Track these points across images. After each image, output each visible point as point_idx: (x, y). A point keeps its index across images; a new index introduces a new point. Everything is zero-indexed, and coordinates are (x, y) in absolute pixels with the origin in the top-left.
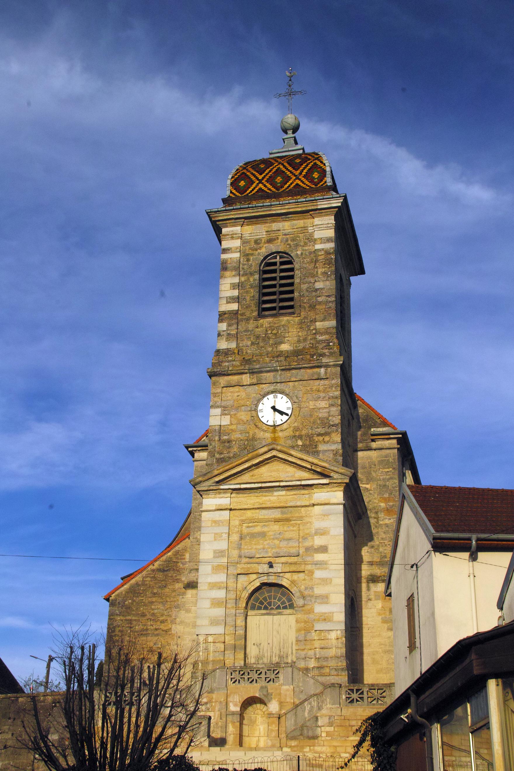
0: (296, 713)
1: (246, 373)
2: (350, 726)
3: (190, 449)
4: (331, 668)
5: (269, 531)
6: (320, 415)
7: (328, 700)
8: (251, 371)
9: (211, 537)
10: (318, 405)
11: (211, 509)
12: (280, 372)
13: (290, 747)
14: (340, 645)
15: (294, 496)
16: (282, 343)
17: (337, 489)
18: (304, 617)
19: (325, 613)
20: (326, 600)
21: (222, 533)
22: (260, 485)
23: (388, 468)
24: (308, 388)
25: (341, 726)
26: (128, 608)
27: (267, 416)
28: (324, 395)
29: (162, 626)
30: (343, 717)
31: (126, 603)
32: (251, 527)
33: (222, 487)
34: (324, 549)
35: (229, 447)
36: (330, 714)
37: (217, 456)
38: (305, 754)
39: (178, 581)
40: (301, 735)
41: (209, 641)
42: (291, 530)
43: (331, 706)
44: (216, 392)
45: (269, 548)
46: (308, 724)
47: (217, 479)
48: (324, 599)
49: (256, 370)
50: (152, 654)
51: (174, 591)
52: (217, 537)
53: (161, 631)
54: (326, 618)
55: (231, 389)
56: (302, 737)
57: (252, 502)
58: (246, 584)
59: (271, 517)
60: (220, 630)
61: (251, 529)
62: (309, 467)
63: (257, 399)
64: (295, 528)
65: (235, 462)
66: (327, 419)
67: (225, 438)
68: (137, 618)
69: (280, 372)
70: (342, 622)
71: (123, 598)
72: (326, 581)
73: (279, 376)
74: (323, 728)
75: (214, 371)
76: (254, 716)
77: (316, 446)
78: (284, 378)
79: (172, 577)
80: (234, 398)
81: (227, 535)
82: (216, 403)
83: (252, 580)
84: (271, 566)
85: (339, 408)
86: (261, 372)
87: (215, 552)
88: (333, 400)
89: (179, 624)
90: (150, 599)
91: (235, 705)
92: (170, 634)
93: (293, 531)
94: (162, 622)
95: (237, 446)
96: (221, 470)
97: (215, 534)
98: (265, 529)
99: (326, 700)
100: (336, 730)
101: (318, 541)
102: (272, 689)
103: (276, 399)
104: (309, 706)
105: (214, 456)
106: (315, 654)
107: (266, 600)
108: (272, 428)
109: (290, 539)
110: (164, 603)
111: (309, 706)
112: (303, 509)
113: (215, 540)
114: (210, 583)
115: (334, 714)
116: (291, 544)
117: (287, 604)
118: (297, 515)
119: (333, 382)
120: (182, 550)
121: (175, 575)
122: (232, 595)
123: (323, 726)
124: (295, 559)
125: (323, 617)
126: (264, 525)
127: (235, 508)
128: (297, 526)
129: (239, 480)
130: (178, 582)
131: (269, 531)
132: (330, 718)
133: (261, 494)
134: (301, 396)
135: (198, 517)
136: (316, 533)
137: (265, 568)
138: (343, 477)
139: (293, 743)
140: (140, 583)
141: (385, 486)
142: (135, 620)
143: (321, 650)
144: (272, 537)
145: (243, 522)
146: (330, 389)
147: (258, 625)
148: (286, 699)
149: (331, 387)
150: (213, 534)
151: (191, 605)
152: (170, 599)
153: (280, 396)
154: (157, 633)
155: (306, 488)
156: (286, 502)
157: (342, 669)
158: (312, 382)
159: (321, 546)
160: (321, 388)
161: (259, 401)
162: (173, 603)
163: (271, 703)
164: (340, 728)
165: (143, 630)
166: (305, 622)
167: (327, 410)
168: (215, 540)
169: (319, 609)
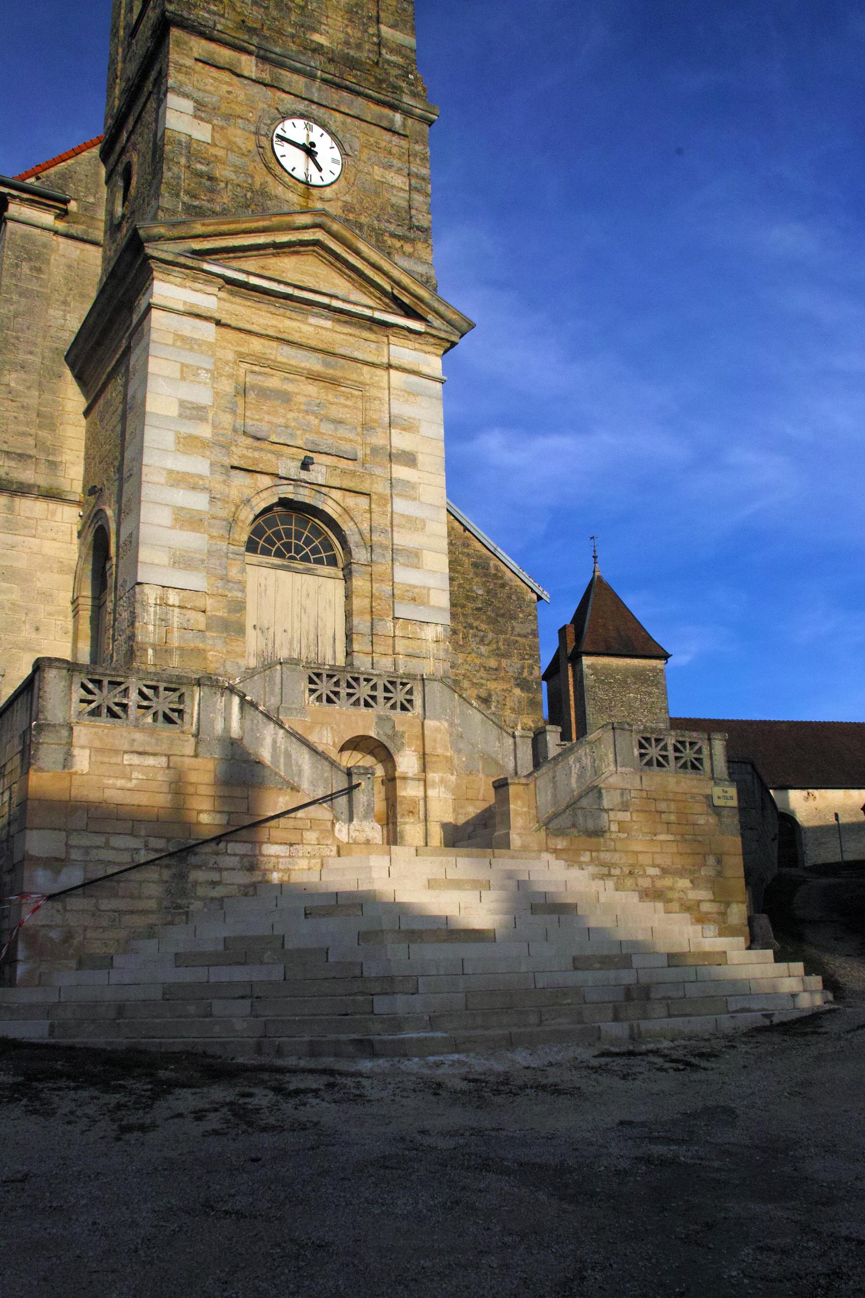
1: (250, 53)
2: (657, 812)
5: (299, 394)
6: (394, 200)
8: (262, 53)
9: (172, 370)
10: (389, 178)
11: (175, 307)
12: (318, 83)
14: (442, 654)
15: (348, 338)
16: (315, 30)
17: (431, 349)
19: (415, 587)
20: (416, 560)
22: (289, 290)
24: (372, 140)
28: (400, 165)
30: (644, 794)
32: (260, 373)
33: (206, 266)
40: (574, 826)
42: (340, 404)
44: (181, 61)
45: (298, 429)
47: (197, 245)
48: (413, 557)
49: (274, 56)
52: (187, 373)
54: (416, 598)
55: (214, 72)
56: (575, 832)
58: (248, 492)
59: (303, 365)
60: (196, 581)
61: (260, 377)
62: (388, 288)
65: (245, 222)
69: (318, 83)
73: (317, 91)
74: (611, 813)
75: (181, 16)
78: (326, 98)
84: (306, 465)
86: (282, 66)
87: (182, 404)
93: (346, 406)
96: (211, 229)
98: (290, 387)
99: (606, 755)
102: (403, 725)
105: (178, 195)
107: (280, 538)
108: (303, 186)
109: (341, 422)
112: (366, 369)
113: (183, 378)
114: (170, 472)
115: (629, 787)
116: (342, 432)
118: (354, 377)
123: (611, 810)
125: (410, 594)
126: (286, 379)
127: (229, 322)
129: (251, 264)
131: (297, 394)
132: (622, 795)
133: (282, 310)
135: (12, 341)
137: (290, 468)
138: (449, 329)
143: (408, 659)
144: (303, 407)
145: (242, 357)
148: (434, 748)
150: (179, 365)
155: (375, 328)
158: (377, 130)
159: (404, 451)
160: (395, 150)
163: (401, 753)
168: (183, 378)
169: (404, 576)
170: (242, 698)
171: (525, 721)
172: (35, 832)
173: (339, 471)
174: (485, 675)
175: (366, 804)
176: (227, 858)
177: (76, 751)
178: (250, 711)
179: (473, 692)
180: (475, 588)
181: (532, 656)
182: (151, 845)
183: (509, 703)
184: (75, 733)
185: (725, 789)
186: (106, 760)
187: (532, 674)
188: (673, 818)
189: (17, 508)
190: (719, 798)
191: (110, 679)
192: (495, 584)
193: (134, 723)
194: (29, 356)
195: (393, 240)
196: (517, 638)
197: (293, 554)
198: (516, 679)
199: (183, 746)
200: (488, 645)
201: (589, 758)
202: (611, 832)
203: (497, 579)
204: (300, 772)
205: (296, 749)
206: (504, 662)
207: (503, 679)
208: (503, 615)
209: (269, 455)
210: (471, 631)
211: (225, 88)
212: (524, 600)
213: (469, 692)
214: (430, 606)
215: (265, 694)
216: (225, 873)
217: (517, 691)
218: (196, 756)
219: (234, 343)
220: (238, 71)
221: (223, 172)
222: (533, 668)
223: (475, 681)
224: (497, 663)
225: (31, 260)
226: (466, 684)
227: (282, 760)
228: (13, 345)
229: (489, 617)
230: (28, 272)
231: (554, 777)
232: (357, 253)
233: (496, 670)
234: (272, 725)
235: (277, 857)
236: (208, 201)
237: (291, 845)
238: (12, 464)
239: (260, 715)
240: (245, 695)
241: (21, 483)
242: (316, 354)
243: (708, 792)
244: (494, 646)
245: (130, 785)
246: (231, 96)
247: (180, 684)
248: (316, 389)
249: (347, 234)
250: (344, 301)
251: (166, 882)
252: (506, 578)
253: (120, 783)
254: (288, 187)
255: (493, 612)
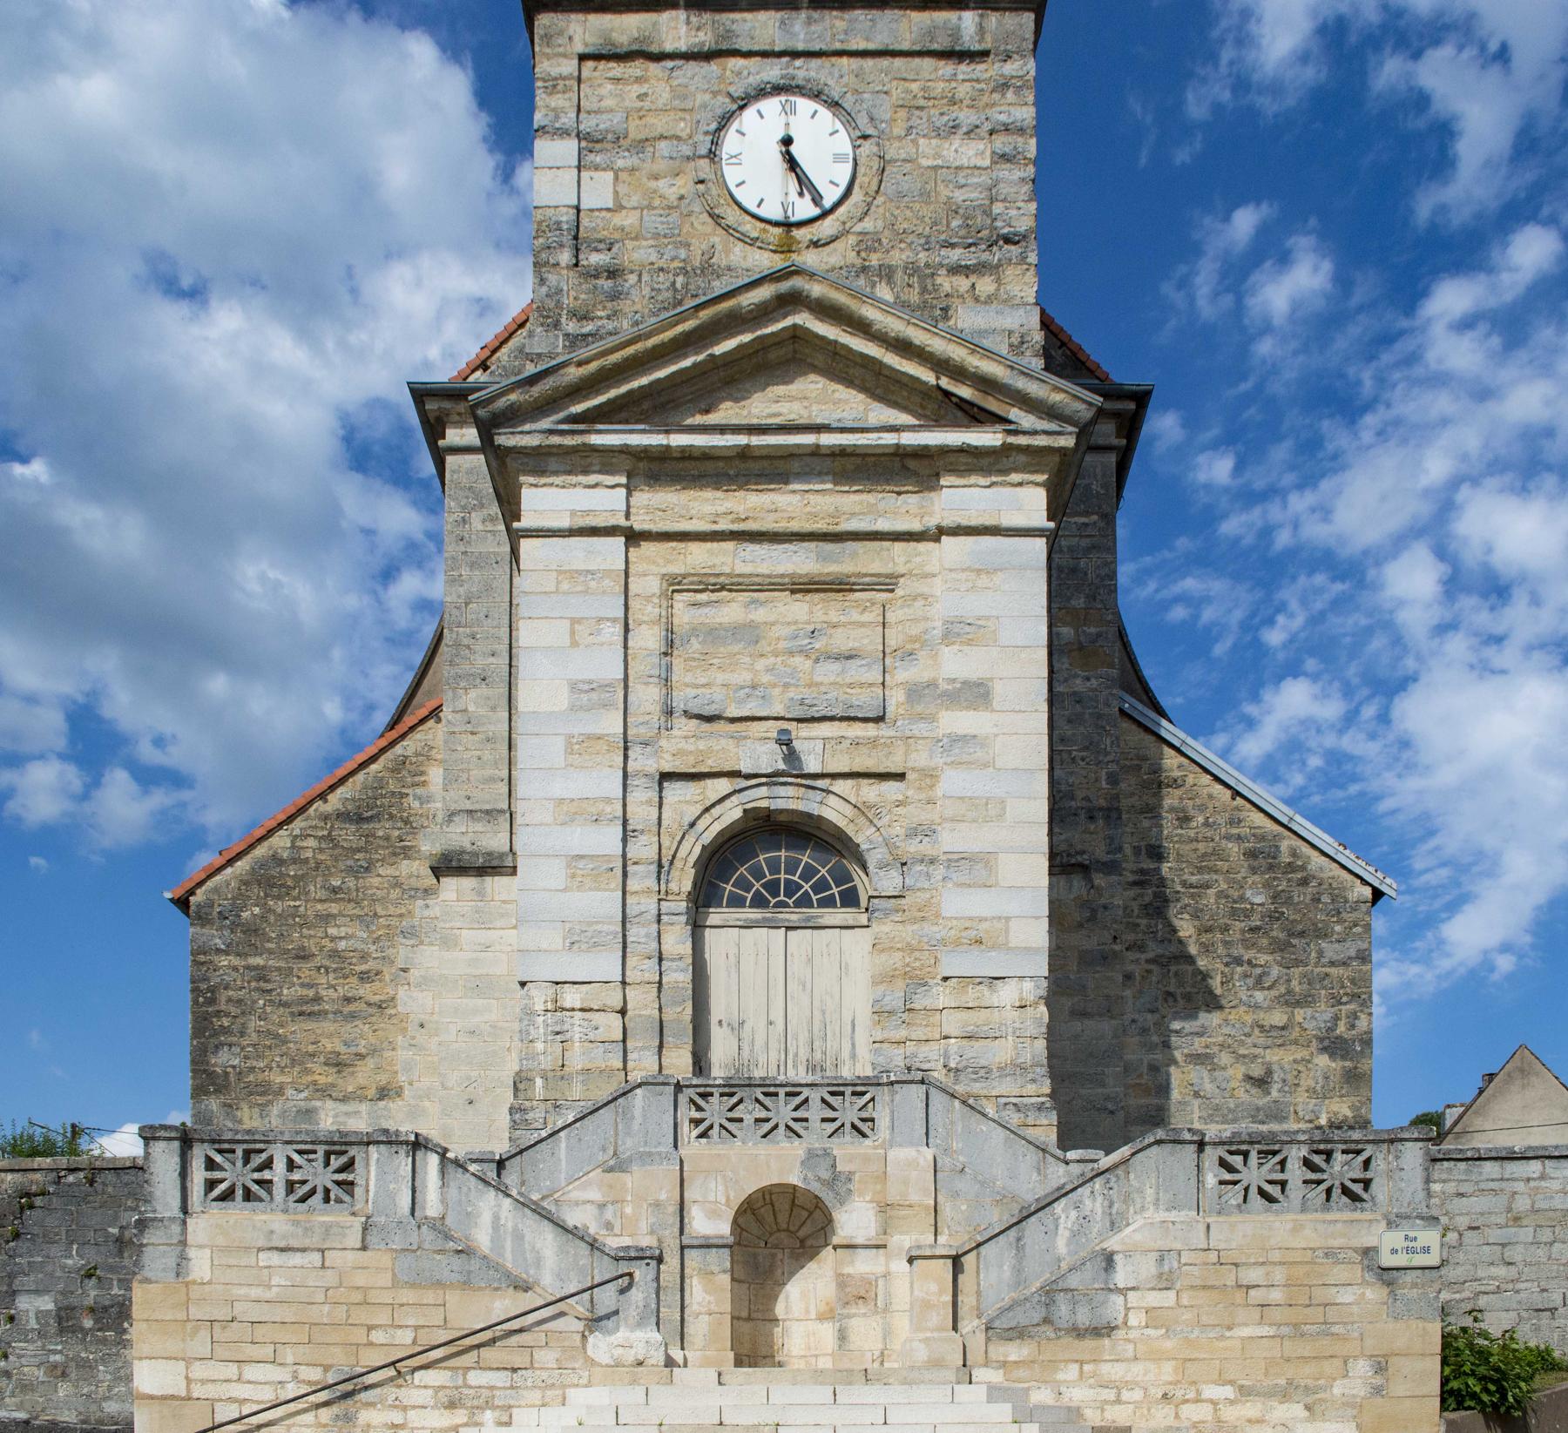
0: (1019, 1239)
3: (431, 406)
4: (1003, 1100)
5: (773, 624)
6: (959, 196)
7: (1150, 1193)
9: (557, 633)
13: (1004, 1364)
18: (908, 933)
21: (600, 620)
23: (1087, 514)
25: (1204, 1287)
26: (252, 930)
27: (757, 182)
29: (365, 991)
30: (1213, 1257)
31: (244, 915)
32: (708, 603)
34: (976, 694)
35: (615, 296)
36: (1161, 1244)
37: (571, 327)
38: (1063, 1389)
39: (407, 853)
40: (1047, 1321)
41: (568, 1005)
43: (1163, 1215)
45: (775, 686)
46: (1073, 1281)
48: (973, 867)
50: (339, 1072)
51: (397, 883)
53: (361, 1006)
55: (616, 69)
57: (708, 509)
59: (781, 570)
63: (719, 112)
64: (867, 617)
66: (987, 213)
67: (595, 259)
68: (282, 964)
70: (1037, 950)
71: (233, 898)
72: (985, 810)
74: (1131, 1294)
76: (767, 1251)
77: (945, 310)
79: (387, 838)
80: (627, 103)
81: (619, 628)
82: (557, 117)
83: (714, 797)
85: (1031, 170)
88: (1010, 139)
89: (419, 985)
90: (319, 906)
91: (713, 1214)
92: (391, 1016)
93: (863, 625)
94: (364, 977)
95: (646, 291)
97: (574, 621)
98: (760, 615)
99: (1141, 1191)
100: (1185, 1302)
101: (955, 664)
103: (792, 119)
104: (1073, 1214)
105: (557, 325)
106: (946, 1056)
108: (778, 231)
110: (366, 920)
111: (1073, 1214)
113: (574, 644)
115: (1178, 1246)
117: (835, 890)
119: (1010, 68)
120: (417, 754)
121: (397, 833)
122: (644, 848)
123: (1133, 1289)
124: (870, 730)
125: (972, 934)
126: (754, 602)
128: (878, 610)
130: (407, 857)
131: (773, 624)
132: (1161, 1259)
134: (887, 116)
135: (465, 641)
136: (948, 637)
139: (1015, 1351)
140: (285, 855)
141: (1074, 570)
142: (279, 969)
144: (782, 645)
145: (675, 584)
146: (996, 96)
147: (732, 959)
149: (1003, 86)
150: (567, 623)
151: (458, 925)
152: (387, 908)
153: (804, 105)
154: (348, 1008)
156: (836, 514)
157: (1040, 1108)
160: (963, 90)
161: (725, 121)
162: (394, 922)
164: (1202, 1293)
165: (304, 1001)
166: (910, 949)
167: (984, 179)
168: (574, 644)
169: (959, 904)
170: (443, 1154)
171: (1335, 1107)
172: (145, 1363)
173: (846, 743)
174: (1261, 1041)
175: (641, 1304)
176: (415, 1392)
177: (192, 1253)
178: (455, 1175)
179: (1239, 1071)
180: (1248, 894)
181: (1355, 997)
182: (301, 1377)
183: (1307, 1082)
184: (190, 1229)
185: (1411, 1234)
186: (233, 1262)
187: (1353, 1026)
188: (1276, 1295)
189: (489, 890)
190: (1394, 1251)
191: (245, 1146)
192: (1289, 880)
193: (282, 1206)
194: (491, 660)
195: (954, 279)
196: (1328, 970)
197: (782, 898)
198: (1321, 1040)
199: (344, 1236)
200: (1269, 988)
201: (1100, 1199)
202: (1130, 1328)
203: (1293, 872)
204: (538, 1263)
205: (530, 1223)
206: (1300, 1014)
207: (1296, 1042)
208: (1302, 934)
209: (723, 742)
210: (1239, 969)
211: (636, 89)
212: (1346, 901)
213: (1230, 1072)
214: (1009, 949)
215: (617, 1134)
216: (411, 1414)
217: (1323, 1060)
218: (364, 1248)
219: (661, 561)
220: (654, 49)
221: (638, 254)
222: (1356, 1018)
223: (1242, 1051)
224: (1285, 1017)
225: (482, 506)
226: (1225, 1058)
227: (508, 1244)
228: (468, 647)
229: (1274, 941)
230: (480, 527)
231: (1019, 1239)
232: (862, 327)
233: (1283, 1028)
234: (492, 1193)
235: (492, 1388)
236: (608, 318)
237: (514, 1370)
238: (479, 827)
239: (473, 1179)
240: (446, 1150)
241: (490, 854)
242: (806, 544)
243: (1370, 1241)
244: (1283, 990)
245: (269, 1295)
246: (647, 104)
247: (346, 1144)
248: (806, 607)
249: (841, 298)
250: (843, 430)
251: (325, 1426)
252: (1312, 867)
253: (255, 1292)
254: (752, 242)
255: (1283, 930)
